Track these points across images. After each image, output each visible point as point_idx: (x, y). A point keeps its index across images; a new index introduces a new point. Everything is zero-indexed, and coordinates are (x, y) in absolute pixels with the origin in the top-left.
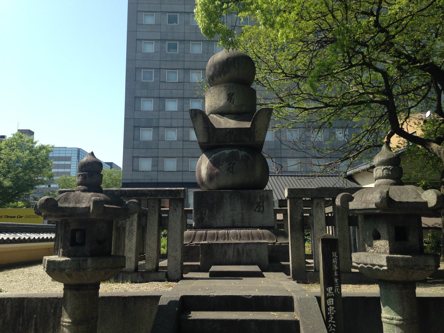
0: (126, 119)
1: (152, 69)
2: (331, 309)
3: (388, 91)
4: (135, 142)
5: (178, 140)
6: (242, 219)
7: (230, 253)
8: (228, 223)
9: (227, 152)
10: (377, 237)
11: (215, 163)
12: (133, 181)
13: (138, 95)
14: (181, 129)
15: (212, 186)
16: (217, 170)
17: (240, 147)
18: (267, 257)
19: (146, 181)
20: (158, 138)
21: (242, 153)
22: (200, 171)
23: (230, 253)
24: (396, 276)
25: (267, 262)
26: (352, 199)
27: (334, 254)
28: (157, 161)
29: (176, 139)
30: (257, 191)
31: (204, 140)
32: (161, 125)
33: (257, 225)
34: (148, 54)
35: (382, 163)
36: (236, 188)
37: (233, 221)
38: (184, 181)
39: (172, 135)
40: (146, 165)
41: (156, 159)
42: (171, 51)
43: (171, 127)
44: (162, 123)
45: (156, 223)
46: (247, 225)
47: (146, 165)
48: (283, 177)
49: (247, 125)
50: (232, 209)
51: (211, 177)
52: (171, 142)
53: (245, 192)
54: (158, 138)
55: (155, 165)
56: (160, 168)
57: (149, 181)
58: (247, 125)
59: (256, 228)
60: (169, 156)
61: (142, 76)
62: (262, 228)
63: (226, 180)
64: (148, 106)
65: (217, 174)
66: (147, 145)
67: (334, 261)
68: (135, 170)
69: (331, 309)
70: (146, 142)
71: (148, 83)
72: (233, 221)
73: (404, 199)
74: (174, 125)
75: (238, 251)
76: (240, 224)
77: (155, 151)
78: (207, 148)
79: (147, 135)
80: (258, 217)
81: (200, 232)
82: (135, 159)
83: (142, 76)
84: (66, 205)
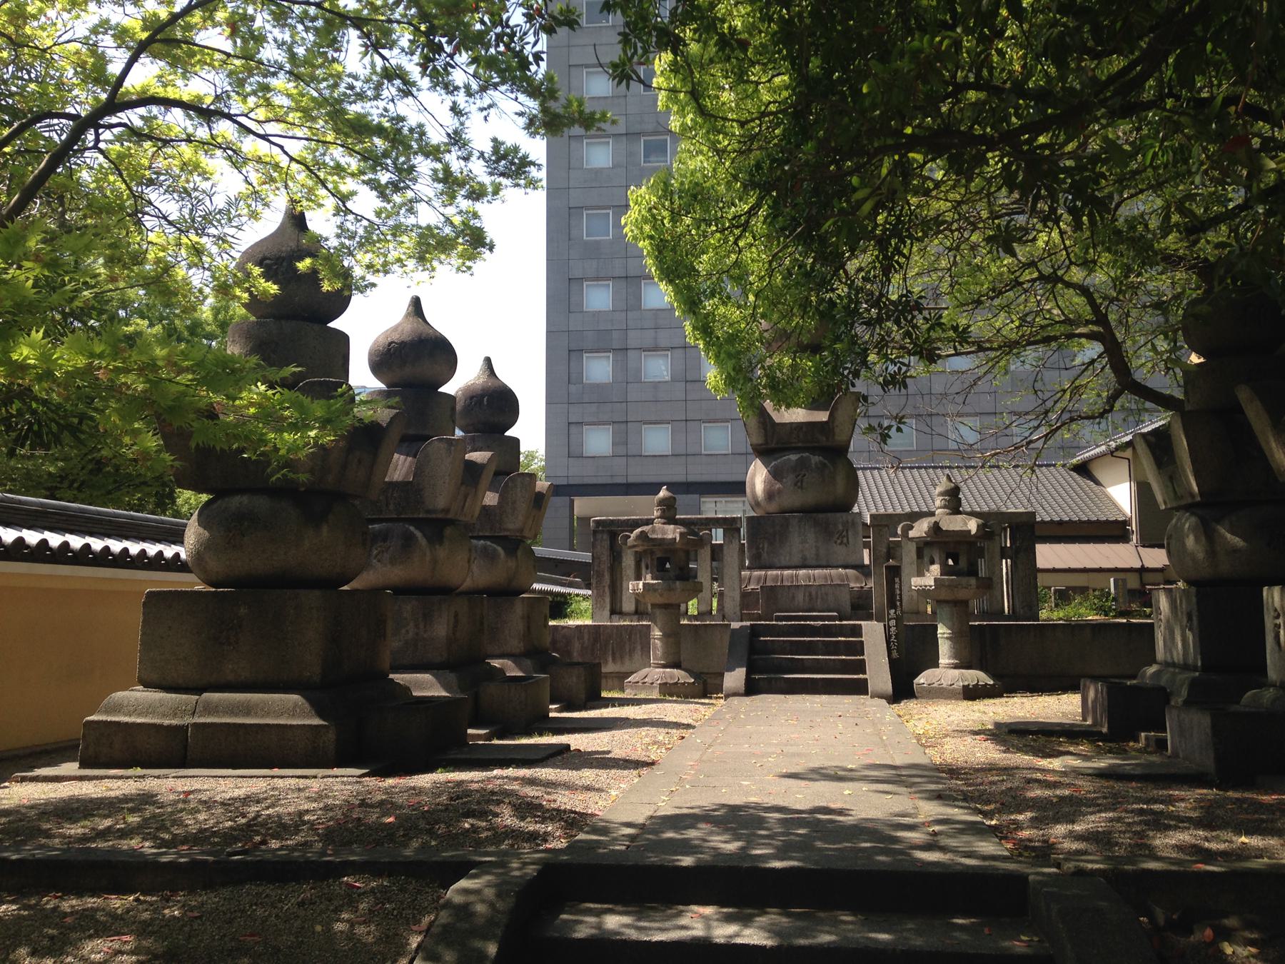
0: (548, 332)
1: (608, 207)
2: (893, 629)
3: (1101, 319)
4: (573, 388)
5: (673, 380)
6: (817, 555)
7: (800, 597)
8: (796, 560)
9: (794, 457)
10: (932, 563)
11: (775, 474)
12: (571, 482)
13: (577, 273)
14: (679, 353)
15: (773, 507)
16: (778, 485)
17: (813, 450)
18: (848, 603)
19: (600, 481)
20: (627, 375)
21: (815, 459)
22: (753, 485)
23: (800, 597)
24: (944, 595)
25: (848, 609)
26: (912, 528)
27: (897, 580)
28: (624, 429)
29: (668, 378)
30: (838, 515)
31: (758, 440)
32: (632, 343)
33: (840, 563)
34: (598, 172)
35: (941, 494)
36: (808, 511)
37: (804, 558)
38: (691, 478)
39: (658, 368)
40: (598, 442)
41: (623, 426)
42: (652, 159)
43: (655, 349)
44: (634, 338)
45: (708, 558)
46: (824, 563)
47: (598, 442)
48: (923, 471)
49: (823, 416)
50: (801, 540)
51: (770, 495)
52: (656, 385)
53: (821, 516)
54: (627, 375)
55: (621, 441)
56: (632, 450)
57: (609, 481)
58: (823, 416)
59: (837, 567)
60: (653, 418)
61: (586, 229)
62: (845, 567)
63: (794, 499)
64: (599, 298)
65: (779, 491)
66: (600, 395)
67: (897, 586)
68: (575, 454)
69: (893, 629)
70: (598, 387)
71: (598, 242)
72: (804, 558)
73: (951, 528)
74: (663, 343)
75: (810, 595)
76: (814, 563)
77: (620, 408)
78: (764, 452)
79: (599, 369)
80: (840, 552)
81: (757, 573)
82: (573, 429)
83: (586, 229)
84: (654, 536)
